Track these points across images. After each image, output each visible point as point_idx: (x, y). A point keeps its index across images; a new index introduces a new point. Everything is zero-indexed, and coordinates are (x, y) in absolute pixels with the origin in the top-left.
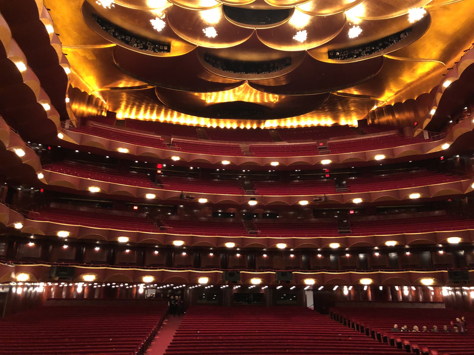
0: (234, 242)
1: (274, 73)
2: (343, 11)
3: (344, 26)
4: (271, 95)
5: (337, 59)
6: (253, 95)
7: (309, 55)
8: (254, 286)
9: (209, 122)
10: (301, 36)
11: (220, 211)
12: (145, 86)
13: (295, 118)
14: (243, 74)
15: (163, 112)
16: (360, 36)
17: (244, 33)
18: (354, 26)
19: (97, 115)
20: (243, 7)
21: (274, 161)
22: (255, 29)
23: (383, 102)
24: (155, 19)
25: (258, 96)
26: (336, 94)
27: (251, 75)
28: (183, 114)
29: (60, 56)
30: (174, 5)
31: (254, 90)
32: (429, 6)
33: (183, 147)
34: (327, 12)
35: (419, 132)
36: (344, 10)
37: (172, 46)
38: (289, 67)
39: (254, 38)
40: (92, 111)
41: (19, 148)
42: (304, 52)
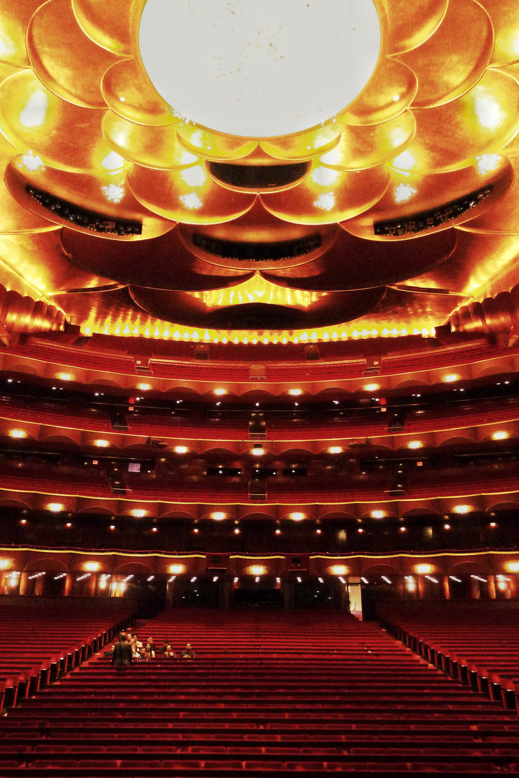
1: (297, 259)
2: (382, 163)
3: (388, 185)
7: (343, 229)
8: (89, 575)
11: (220, 467)
12: (115, 286)
18: (401, 185)
19: (51, 330)
21: (295, 387)
22: (258, 194)
26: (396, 287)
27: (263, 262)
28: (159, 321)
37: (144, 225)
39: (258, 206)
40: (43, 324)
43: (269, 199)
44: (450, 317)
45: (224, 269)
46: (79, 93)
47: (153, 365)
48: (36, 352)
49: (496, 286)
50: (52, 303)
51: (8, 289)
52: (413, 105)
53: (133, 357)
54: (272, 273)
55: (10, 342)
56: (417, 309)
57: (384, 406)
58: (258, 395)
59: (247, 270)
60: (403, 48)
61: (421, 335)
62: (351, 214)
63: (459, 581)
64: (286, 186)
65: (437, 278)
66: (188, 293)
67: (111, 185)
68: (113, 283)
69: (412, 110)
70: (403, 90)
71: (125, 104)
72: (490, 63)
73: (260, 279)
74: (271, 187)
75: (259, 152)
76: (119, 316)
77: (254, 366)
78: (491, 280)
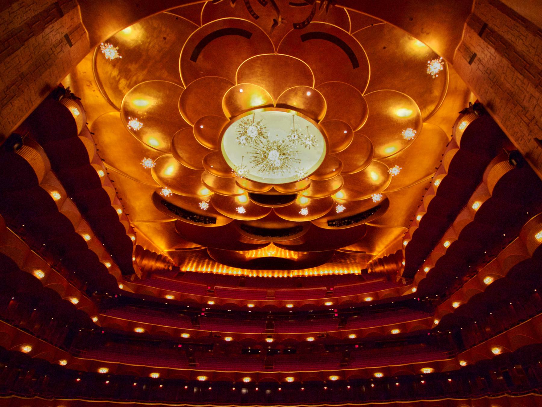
0: (250, 377)
1: (291, 236)
4: (292, 252)
5: (334, 226)
6: (279, 253)
9: (250, 273)
10: (304, 212)
11: (249, 348)
12: (200, 248)
13: (315, 268)
14: (269, 237)
15: (216, 266)
16: (345, 211)
17: (264, 211)
19: (164, 269)
20: (262, 194)
23: (376, 256)
24: (202, 203)
25: (288, 254)
27: (275, 238)
28: (231, 268)
29: (127, 229)
30: (215, 194)
31: (280, 249)
32: (385, 192)
33: (219, 293)
34: (319, 196)
35: (399, 279)
36: (330, 194)
38: (301, 233)
40: (160, 265)
41: (74, 297)
42: (309, 222)
43: (280, 211)
44: (368, 264)
45: (256, 241)
46: (192, 163)
47: (216, 289)
48: (156, 283)
49: (387, 251)
50: (167, 255)
51: (145, 249)
52: (342, 172)
53: (206, 285)
54: (279, 243)
55: (142, 277)
56: (351, 261)
57: (336, 313)
58: (270, 307)
59: (267, 241)
60: (336, 151)
61: (354, 274)
62: (316, 217)
63: (230, 310)
64: (288, 204)
65: (360, 246)
66: (237, 252)
67: (203, 202)
68: (199, 246)
69: (341, 175)
70: (337, 167)
71: (212, 168)
72: (373, 158)
73: (273, 246)
74: (279, 204)
75: (273, 190)
76: (200, 262)
77: (269, 290)
78: (385, 247)
